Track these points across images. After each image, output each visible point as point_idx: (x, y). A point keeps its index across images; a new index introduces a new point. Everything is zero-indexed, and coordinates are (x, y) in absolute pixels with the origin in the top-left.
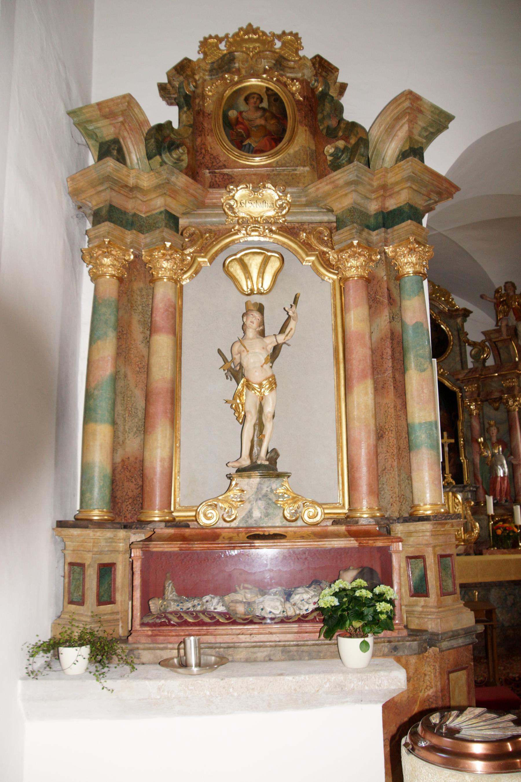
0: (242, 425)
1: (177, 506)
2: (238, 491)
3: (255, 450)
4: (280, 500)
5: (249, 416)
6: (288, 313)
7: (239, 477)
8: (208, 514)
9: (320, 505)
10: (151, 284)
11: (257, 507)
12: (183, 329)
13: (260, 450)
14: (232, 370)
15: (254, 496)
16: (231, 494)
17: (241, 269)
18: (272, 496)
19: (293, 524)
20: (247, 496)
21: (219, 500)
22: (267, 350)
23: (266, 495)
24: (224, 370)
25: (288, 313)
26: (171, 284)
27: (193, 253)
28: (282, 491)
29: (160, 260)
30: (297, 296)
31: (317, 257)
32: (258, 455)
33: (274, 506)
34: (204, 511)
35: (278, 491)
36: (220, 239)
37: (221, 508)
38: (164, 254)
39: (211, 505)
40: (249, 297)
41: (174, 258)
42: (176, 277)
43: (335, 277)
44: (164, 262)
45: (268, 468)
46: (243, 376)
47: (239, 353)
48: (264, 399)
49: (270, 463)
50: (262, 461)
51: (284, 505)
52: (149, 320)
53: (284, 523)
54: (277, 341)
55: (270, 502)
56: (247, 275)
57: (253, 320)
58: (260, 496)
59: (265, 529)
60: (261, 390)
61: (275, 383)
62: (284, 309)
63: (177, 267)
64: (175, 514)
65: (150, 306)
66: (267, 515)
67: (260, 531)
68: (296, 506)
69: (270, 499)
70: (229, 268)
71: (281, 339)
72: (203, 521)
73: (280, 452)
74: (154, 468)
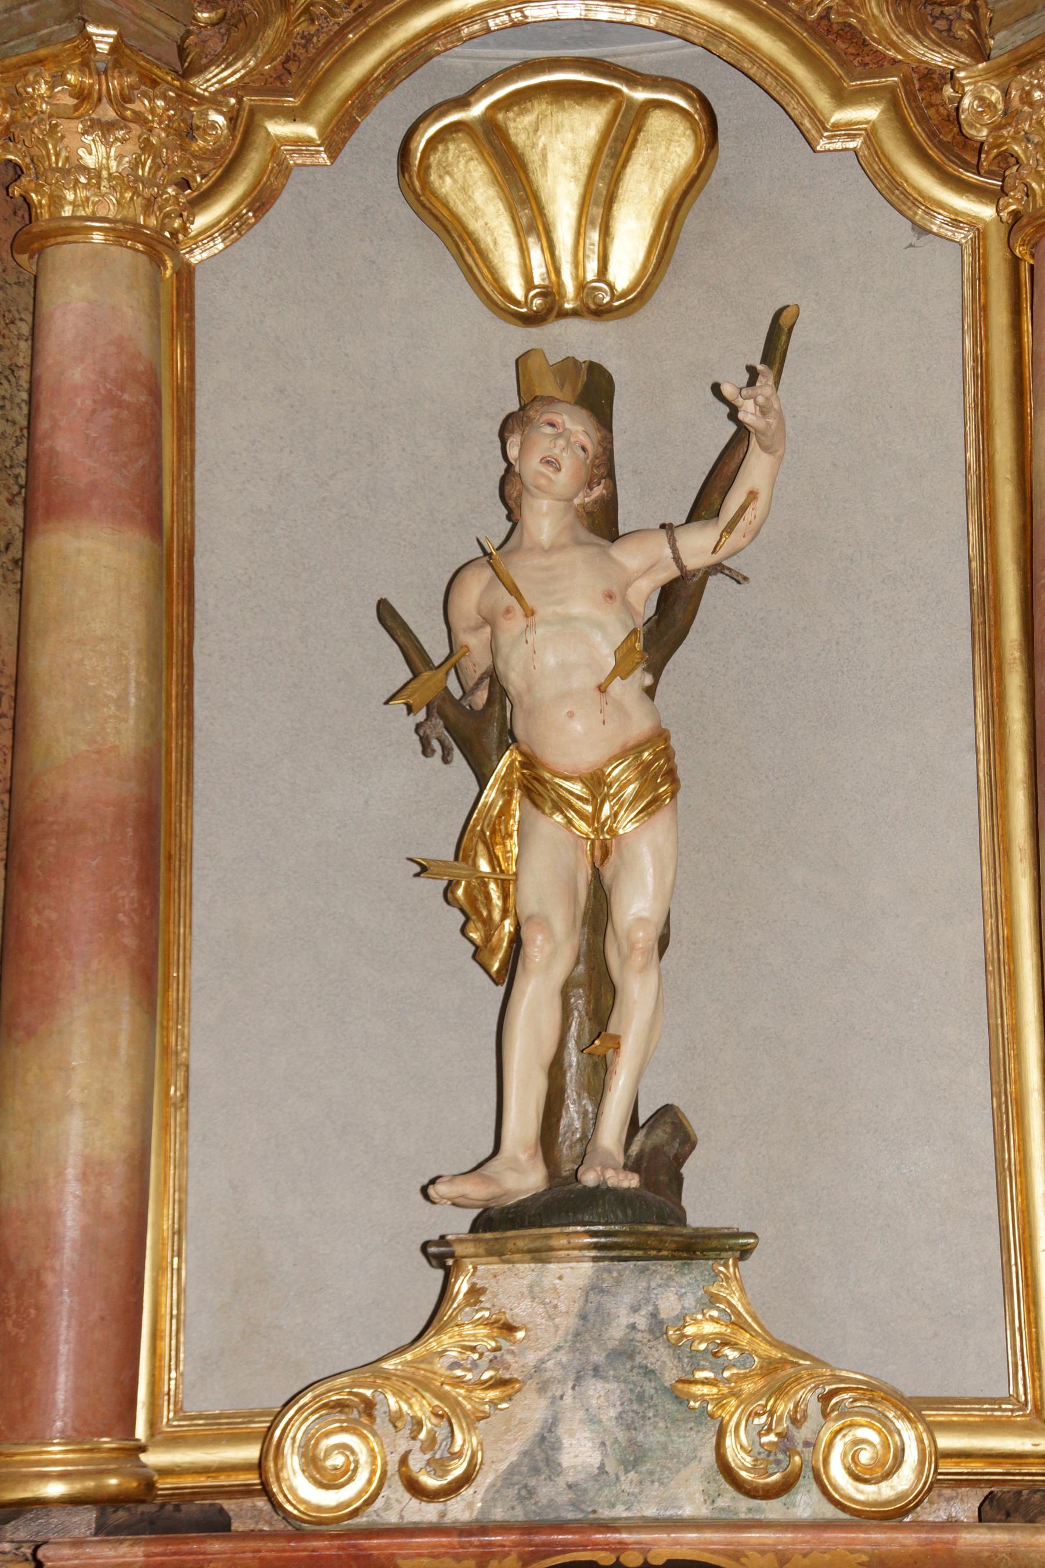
0: (502, 989)
1: (167, 1414)
2: (483, 1331)
3: (572, 1114)
4: (700, 1375)
5: (539, 939)
6: (733, 413)
7: (490, 1253)
8: (328, 1453)
9: (913, 1408)
10: (23, 259)
11: (581, 1414)
12: (198, 497)
13: (597, 1116)
14: (449, 710)
15: (563, 1357)
16: (445, 1342)
17: (495, 181)
18: (659, 1357)
19: (772, 1509)
20: (531, 1358)
21: (387, 1376)
22: (627, 607)
23: (625, 1352)
24: (410, 709)
25: (733, 413)
26: (127, 258)
27: (238, 90)
28: (709, 1328)
29: (64, 125)
30: (785, 320)
31: (894, 106)
32: (588, 1138)
33: (671, 1407)
34: (308, 1437)
35: (689, 1330)
36: (379, 15)
37: (395, 1419)
38: (82, 95)
39: (341, 1406)
40: (533, 330)
41: (139, 118)
42: (153, 222)
43: (986, 212)
44: (88, 139)
45: (637, 1207)
46: (508, 737)
47: (489, 620)
48: (613, 857)
49: (645, 1183)
50: (608, 1170)
51: (720, 1401)
52: (21, 452)
53: (721, 1503)
54: (677, 559)
55: (649, 1388)
56: (524, 215)
57: (557, 450)
58: (598, 1357)
59: (625, 1536)
60: (598, 810)
61: (671, 775)
62: (716, 389)
63: (156, 167)
64: (152, 1458)
65: (24, 375)
66: (634, 1457)
67: (596, 1546)
68: (785, 1408)
69: (648, 1373)
70: (433, 177)
71: (698, 546)
72: (301, 1490)
73: (696, 1122)
74: (49, 1217)
